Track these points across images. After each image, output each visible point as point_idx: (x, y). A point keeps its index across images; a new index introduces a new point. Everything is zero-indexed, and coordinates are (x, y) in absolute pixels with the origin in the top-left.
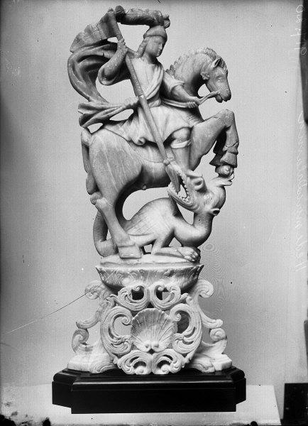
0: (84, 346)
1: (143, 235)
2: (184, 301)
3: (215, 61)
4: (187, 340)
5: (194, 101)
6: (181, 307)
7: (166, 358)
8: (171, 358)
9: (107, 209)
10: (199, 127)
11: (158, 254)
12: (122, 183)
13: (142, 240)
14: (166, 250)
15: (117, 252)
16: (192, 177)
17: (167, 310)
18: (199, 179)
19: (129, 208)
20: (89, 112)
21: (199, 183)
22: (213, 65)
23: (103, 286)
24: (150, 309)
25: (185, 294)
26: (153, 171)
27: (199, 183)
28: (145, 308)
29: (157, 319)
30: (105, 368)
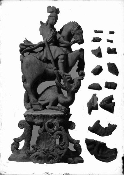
0: (17, 150)
1: (44, 100)
2: (60, 130)
3: (77, 26)
4: (62, 148)
5: (67, 43)
6: (59, 132)
7: (51, 156)
8: (54, 156)
9: (28, 88)
10: (70, 55)
11: (50, 109)
12: (52, 154)
13: (42, 103)
14: (53, 107)
15: (32, 107)
16: (66, 76)
17: (52, 134)
18: (69, 76)
19: (40, 90)
20: (25, 47)
21: (68, 78)
22: (76, 29)
23: (26, 123)
24: (45, 133)
25: (61, 127)
26: (52, 72)
27: (68, 78)
28: (42, 132)
29: (48, 137)
30: (50, 30)
